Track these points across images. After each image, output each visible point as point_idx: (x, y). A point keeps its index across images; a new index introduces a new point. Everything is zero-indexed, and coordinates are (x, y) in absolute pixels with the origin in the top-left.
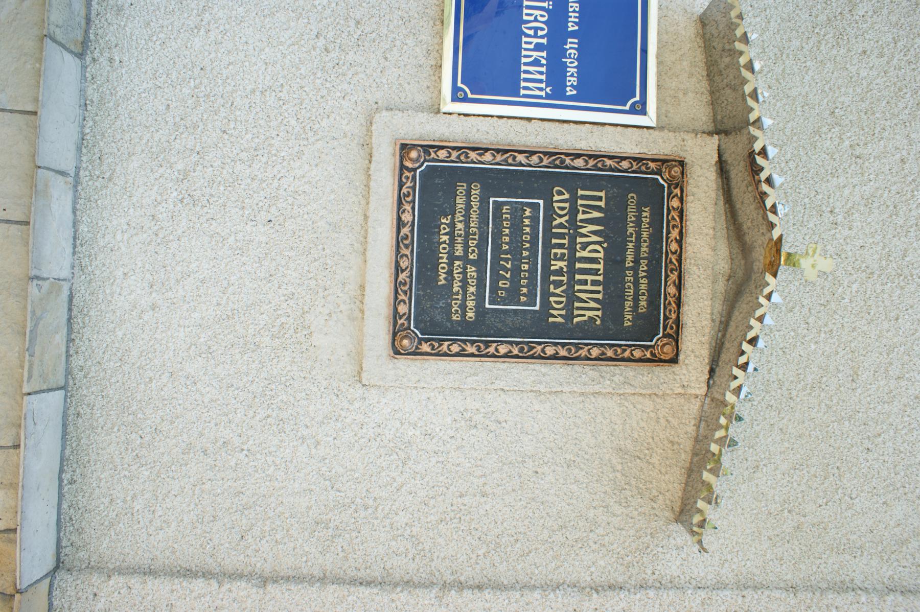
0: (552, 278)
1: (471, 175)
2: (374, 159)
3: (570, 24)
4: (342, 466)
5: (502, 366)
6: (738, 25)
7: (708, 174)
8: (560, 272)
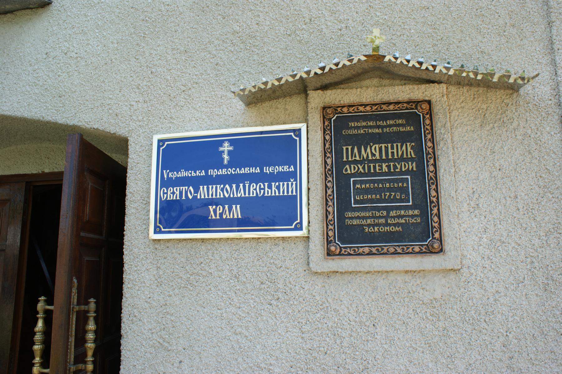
0: (392, 170)
1: (341, 218)
2: (336, 270)
3: (256, 172)
4: (509, 277)
5: (442, 193)
6: (259, 88)
7: (328, 94)
8: (389, 167)
